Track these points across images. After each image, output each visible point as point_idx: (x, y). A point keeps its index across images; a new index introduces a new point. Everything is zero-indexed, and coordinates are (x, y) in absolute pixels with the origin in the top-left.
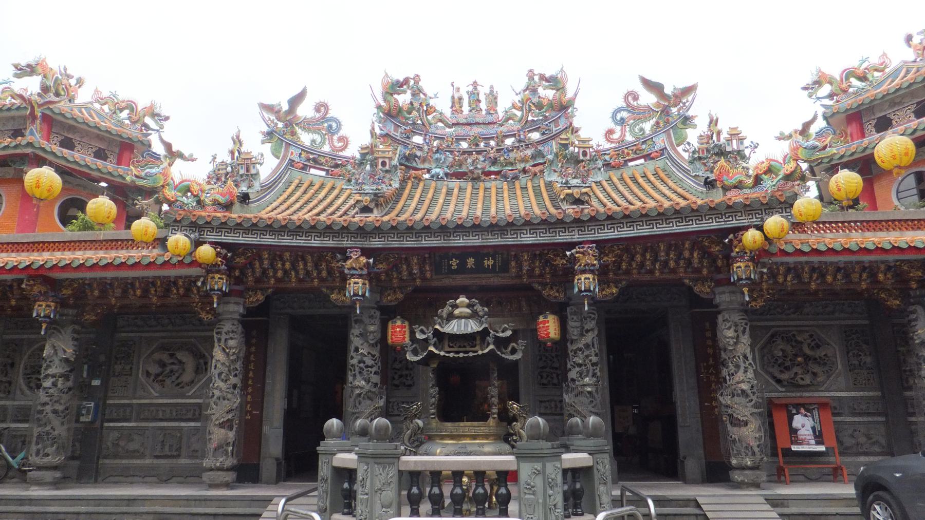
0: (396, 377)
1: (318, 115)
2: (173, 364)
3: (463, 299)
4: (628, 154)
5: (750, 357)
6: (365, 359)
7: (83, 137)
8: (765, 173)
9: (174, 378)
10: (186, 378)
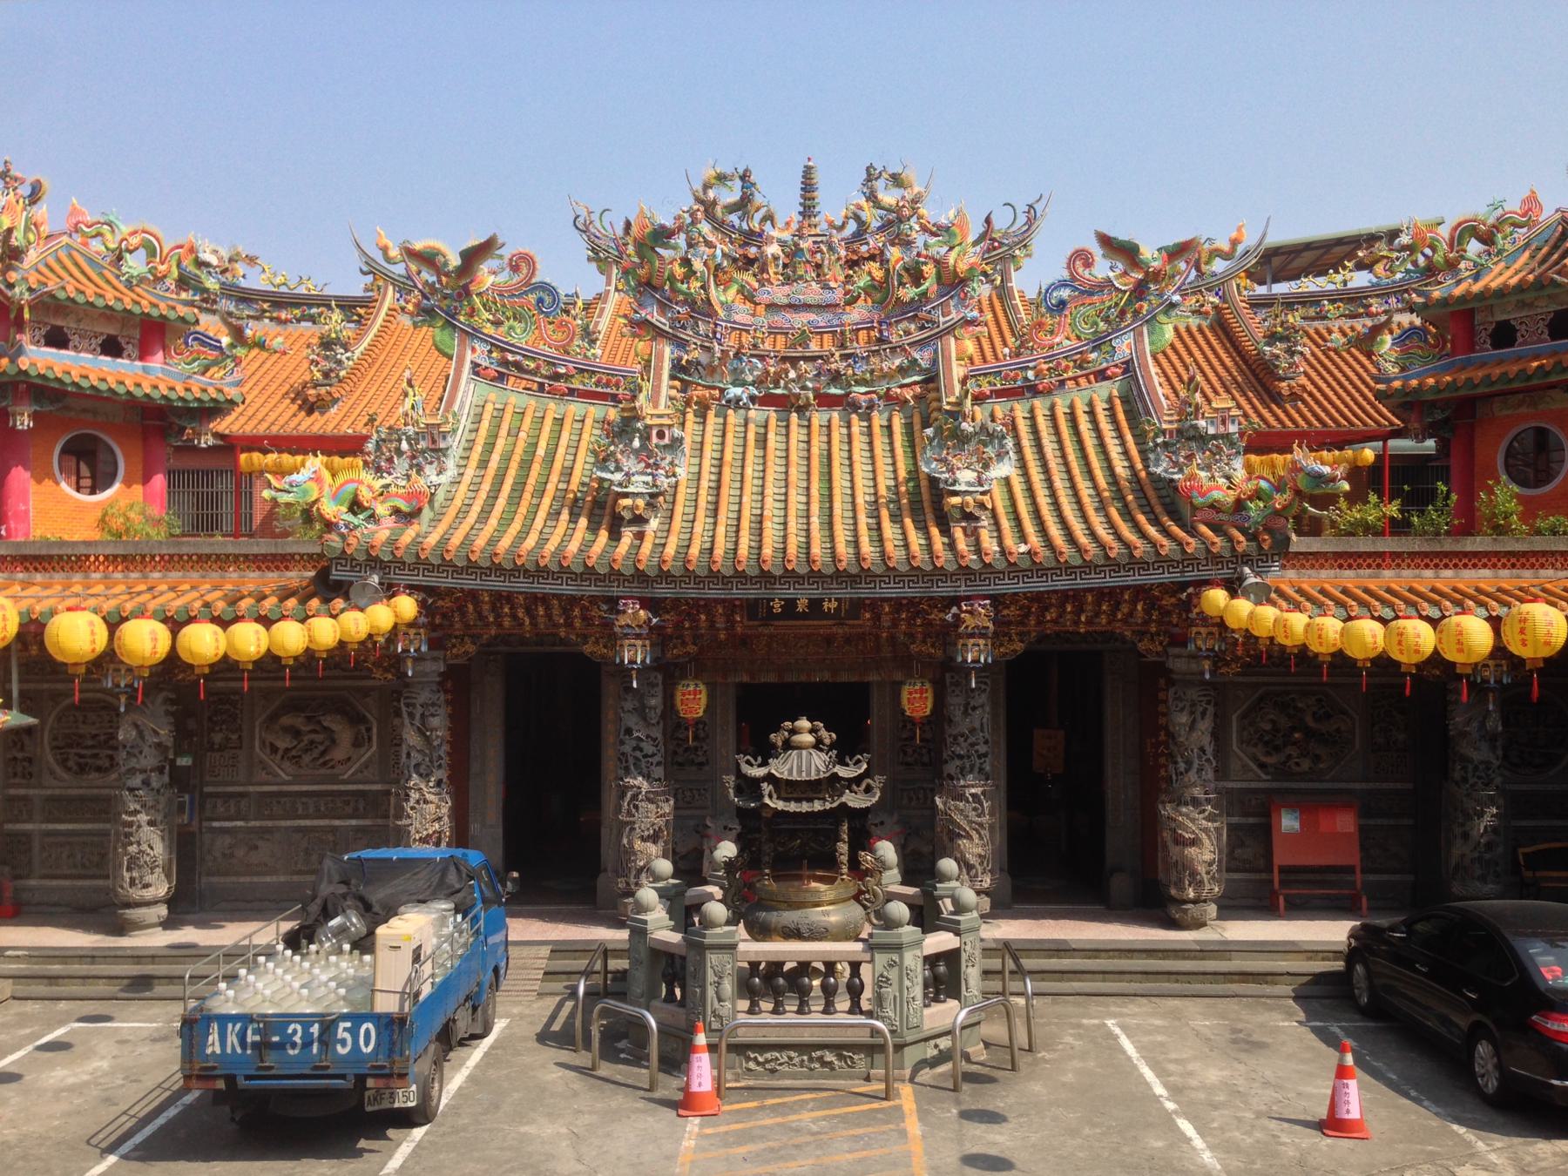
0: (680, 751)
1: (516, 279)
2: (314, 731)
3: (804, 723)
4: (1067, 367)
5: (1209, 750)
6: (643, 745)
7: (79, 321)
8: (1250, 498)
9: (316, 753)
10: (339, 754)
